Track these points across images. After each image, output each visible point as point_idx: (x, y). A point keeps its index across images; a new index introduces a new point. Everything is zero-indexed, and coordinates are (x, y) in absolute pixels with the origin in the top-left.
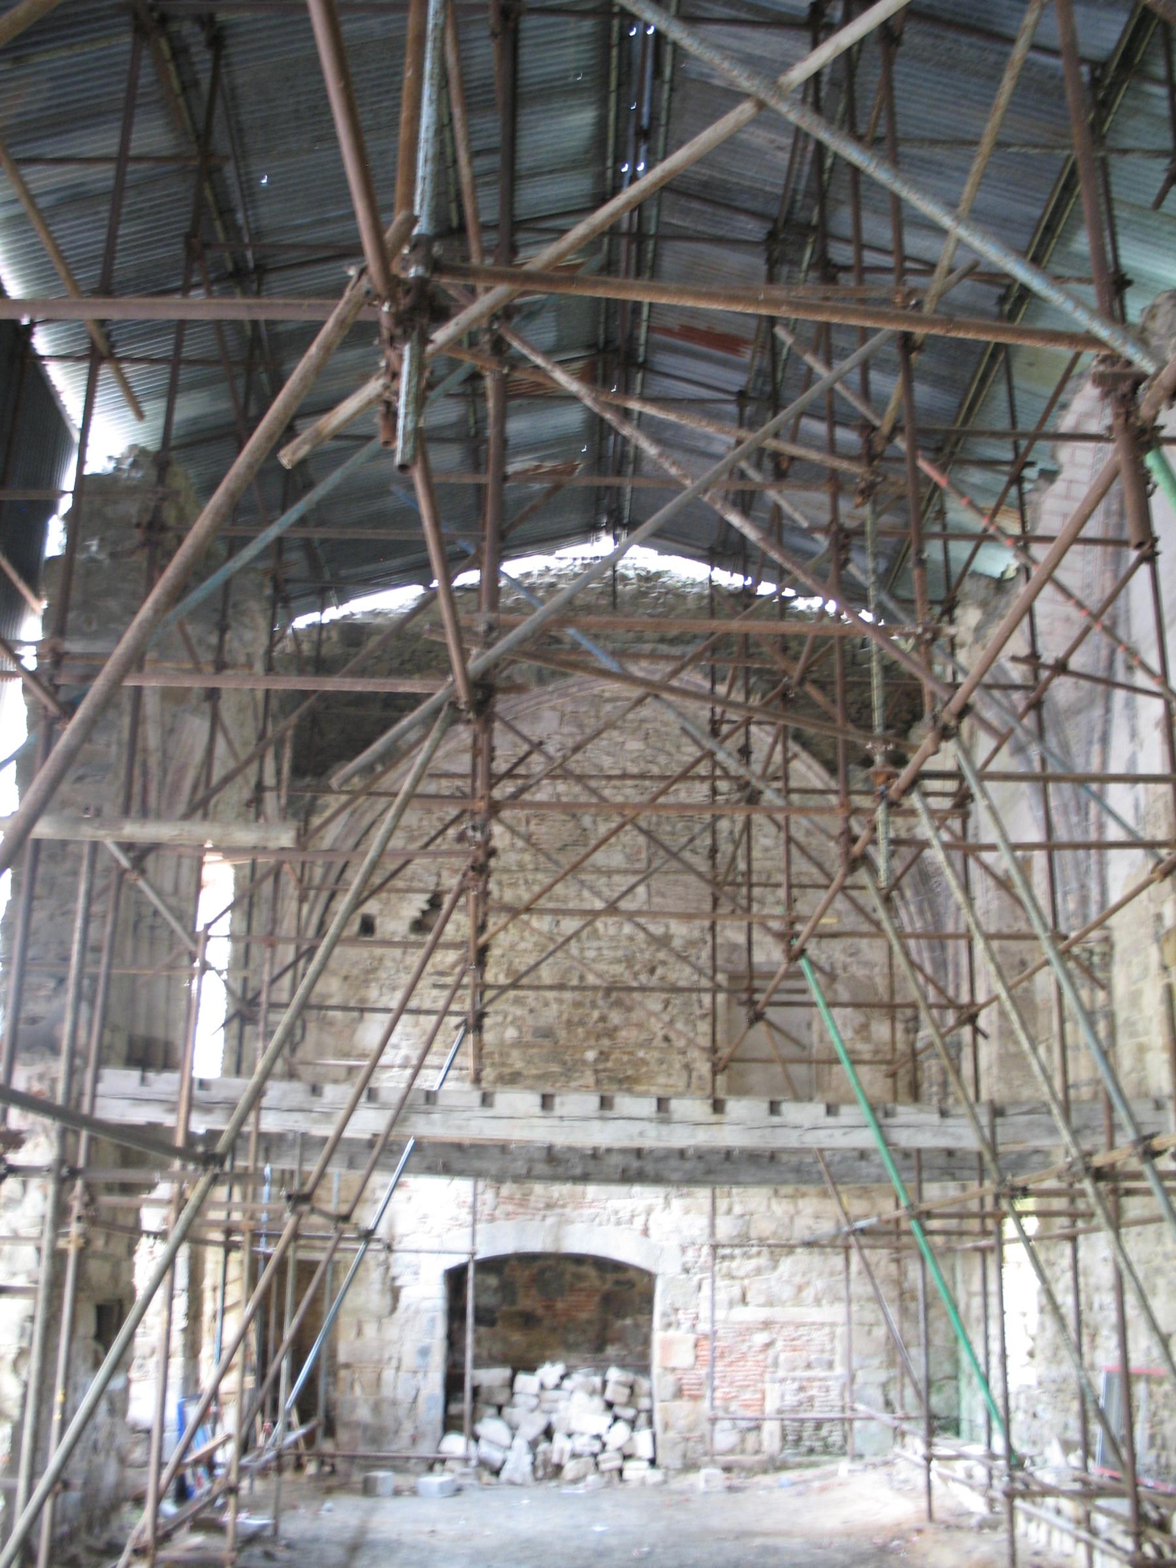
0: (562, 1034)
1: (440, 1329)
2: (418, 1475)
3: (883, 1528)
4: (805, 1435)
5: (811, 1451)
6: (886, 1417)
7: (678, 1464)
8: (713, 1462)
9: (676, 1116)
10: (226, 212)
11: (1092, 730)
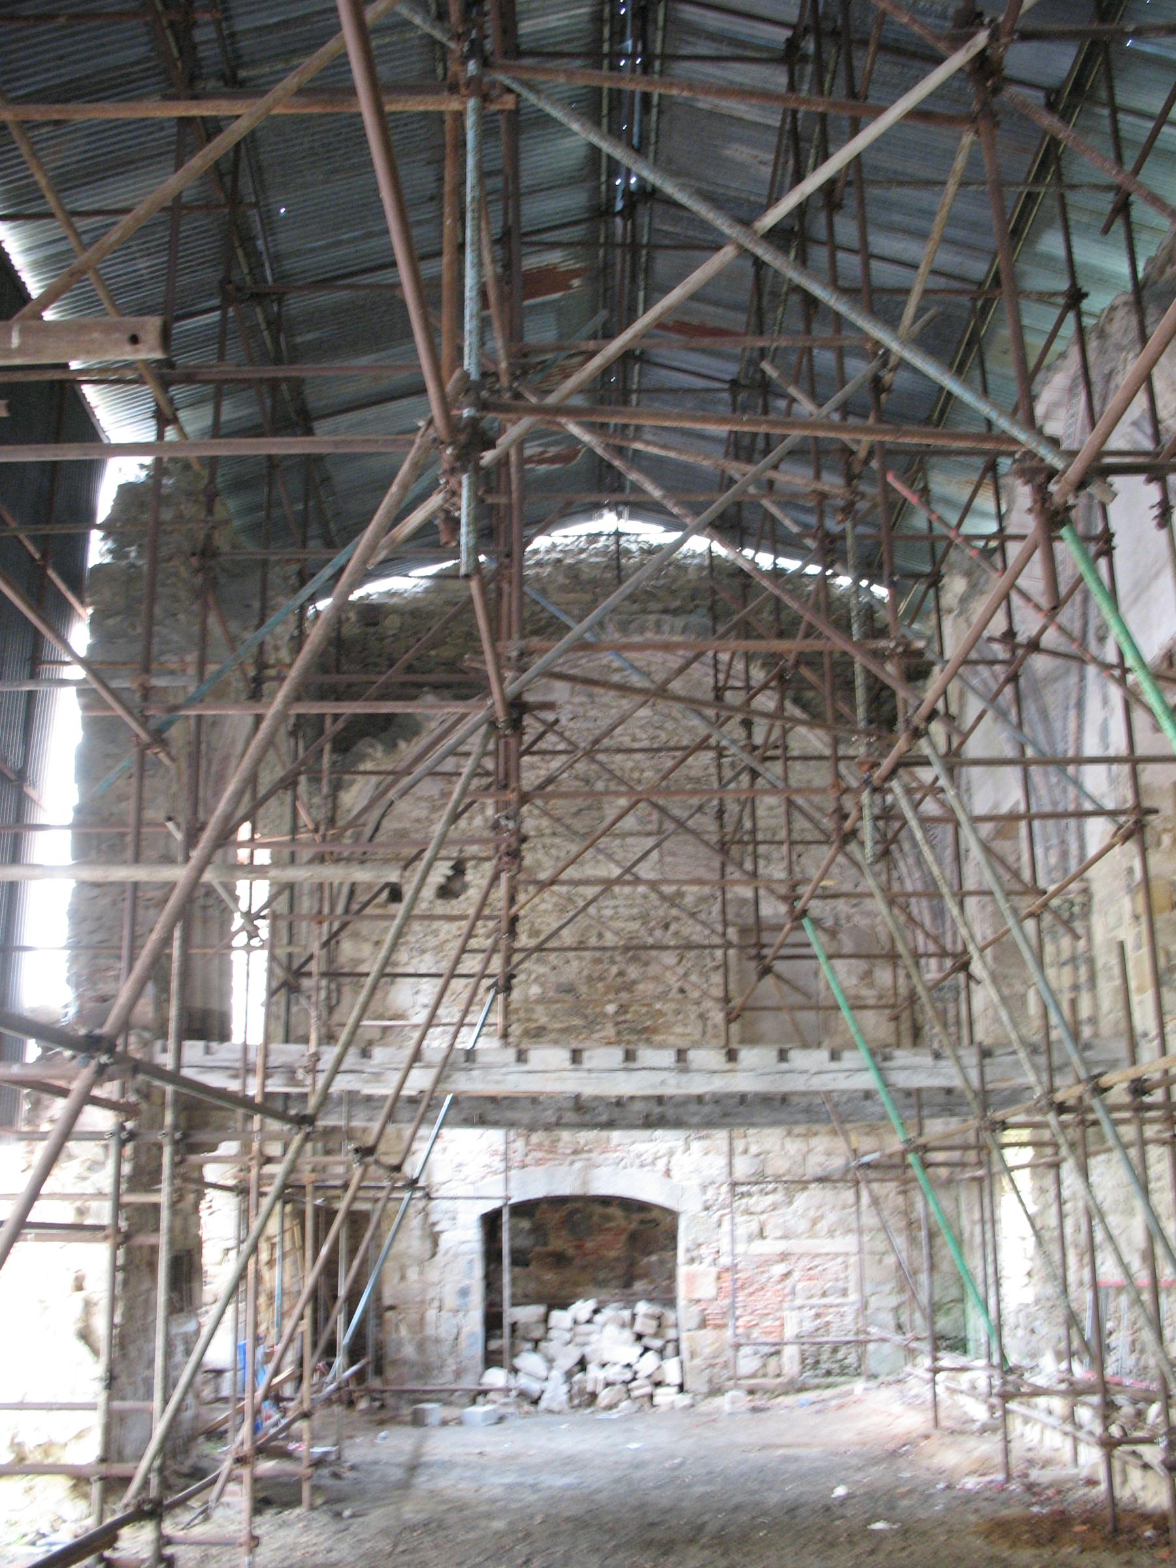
0: (583, 989)
1: (478, 1271)
2: (464, 1406)
3: (894, 1437)
4: (824, 1357)
5: (829, 1373)
6: (898, 1338)
7: (704, 1388)
8: (736, 1387)
9: (694, 1066)
10: (247, 240)
11: (1067, 697)
